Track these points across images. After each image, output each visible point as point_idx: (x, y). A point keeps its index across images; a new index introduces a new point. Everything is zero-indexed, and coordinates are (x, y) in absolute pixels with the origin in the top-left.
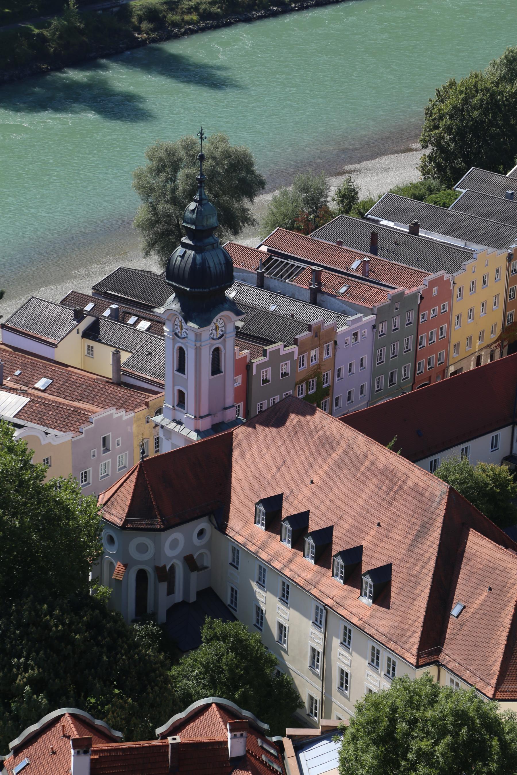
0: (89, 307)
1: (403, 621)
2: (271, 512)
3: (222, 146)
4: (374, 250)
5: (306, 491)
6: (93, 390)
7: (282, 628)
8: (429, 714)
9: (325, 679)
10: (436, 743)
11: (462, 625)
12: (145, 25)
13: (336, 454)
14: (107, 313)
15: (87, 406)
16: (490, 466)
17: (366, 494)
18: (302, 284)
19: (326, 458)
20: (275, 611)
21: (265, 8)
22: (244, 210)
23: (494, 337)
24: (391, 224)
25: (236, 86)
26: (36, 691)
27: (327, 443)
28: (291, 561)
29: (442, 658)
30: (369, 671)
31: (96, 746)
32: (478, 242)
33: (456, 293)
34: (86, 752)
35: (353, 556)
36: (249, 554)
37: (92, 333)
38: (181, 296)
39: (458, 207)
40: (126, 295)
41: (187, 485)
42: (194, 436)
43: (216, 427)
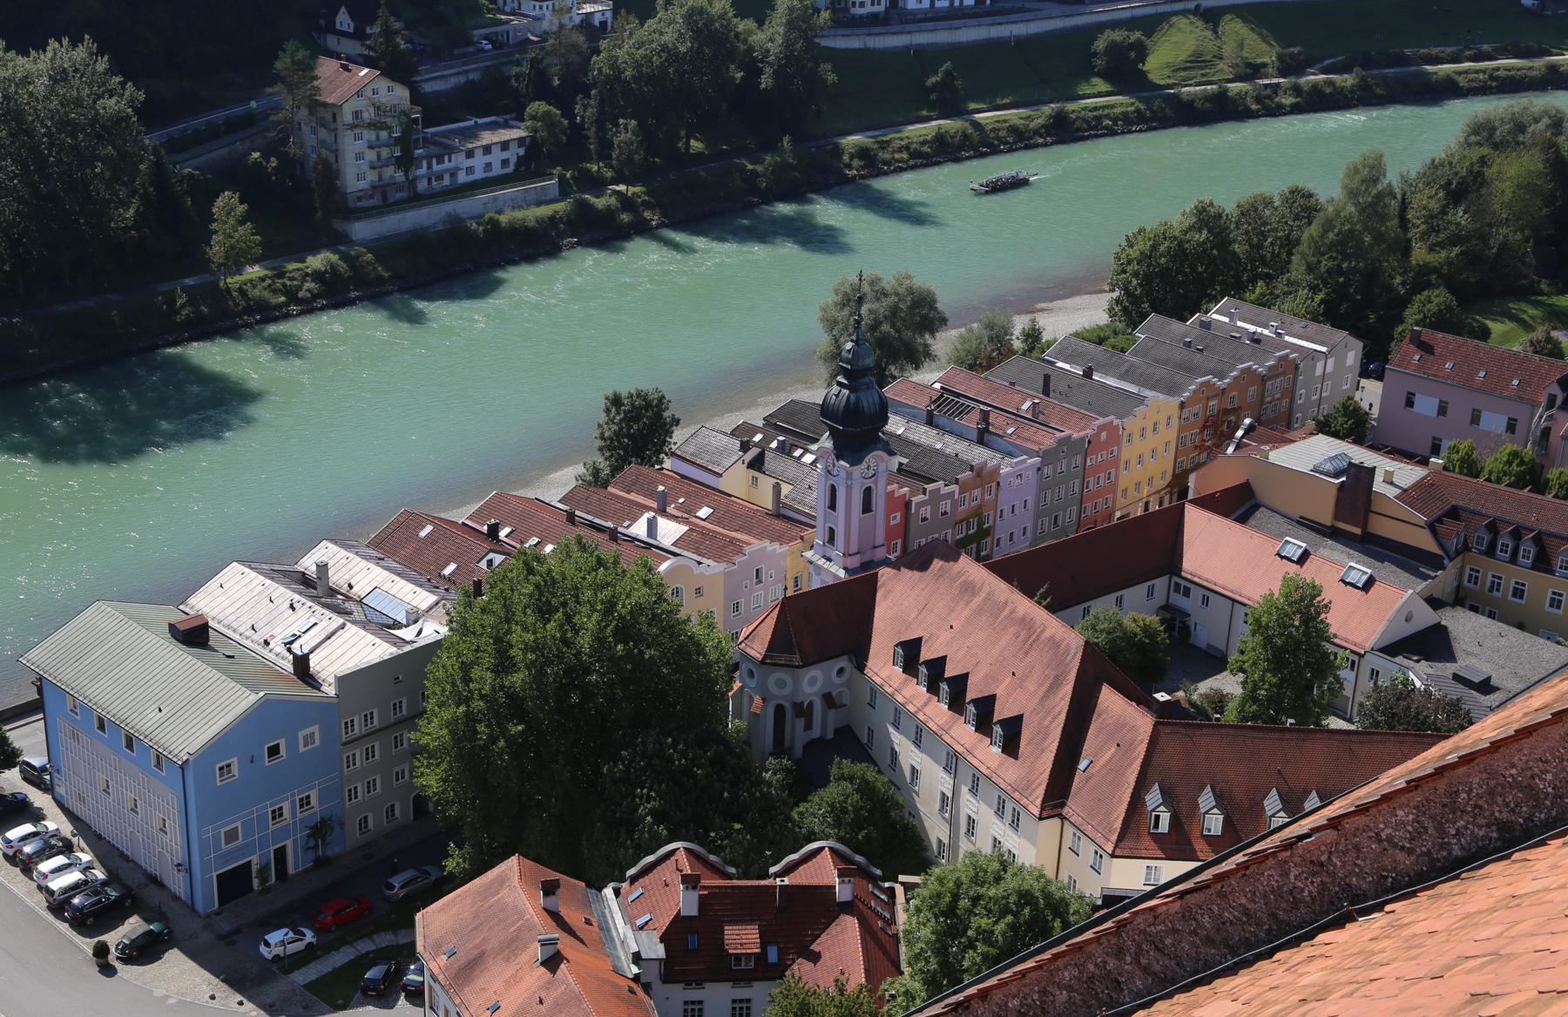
0: (758, 438)
1: (1030, 772)
2: (909, 654)
3: (907, 283)
4: (1046, 392)
5: (945, 636)
6: (750, 521)
7: (914, 770)
8: (992, 892)
9: (953, 823)
10: (996, 923)
11: (1087, 780)
12: (856, 163)
13: (977, 601)
14: (774, 445)
15: (744, 537)
16: (1142, 616)
17: (1002, 643)
18: (971, 422)
19: (967, 604)
20: (909, 755)
21: (975, 149)
22: (926, 346)
23: (1164, 483)
24: (1067, 367)
25: (932, 223)
26: (657, 822)
27: (969, 589)
28: (925, 705)
29: (1065, 811)
30: (995, 819)
31: (704, 882)
32: (1153, 388)
33: (1125, 439)
34: (694, 888)
35: (986, 705)
36: (885, 695)
37: (757, 464)
38: (834, 434)
39: (1135, 354)
40: (791, 428)
41: (829, 624)
42: (842, 574)
43: (865, 566)
